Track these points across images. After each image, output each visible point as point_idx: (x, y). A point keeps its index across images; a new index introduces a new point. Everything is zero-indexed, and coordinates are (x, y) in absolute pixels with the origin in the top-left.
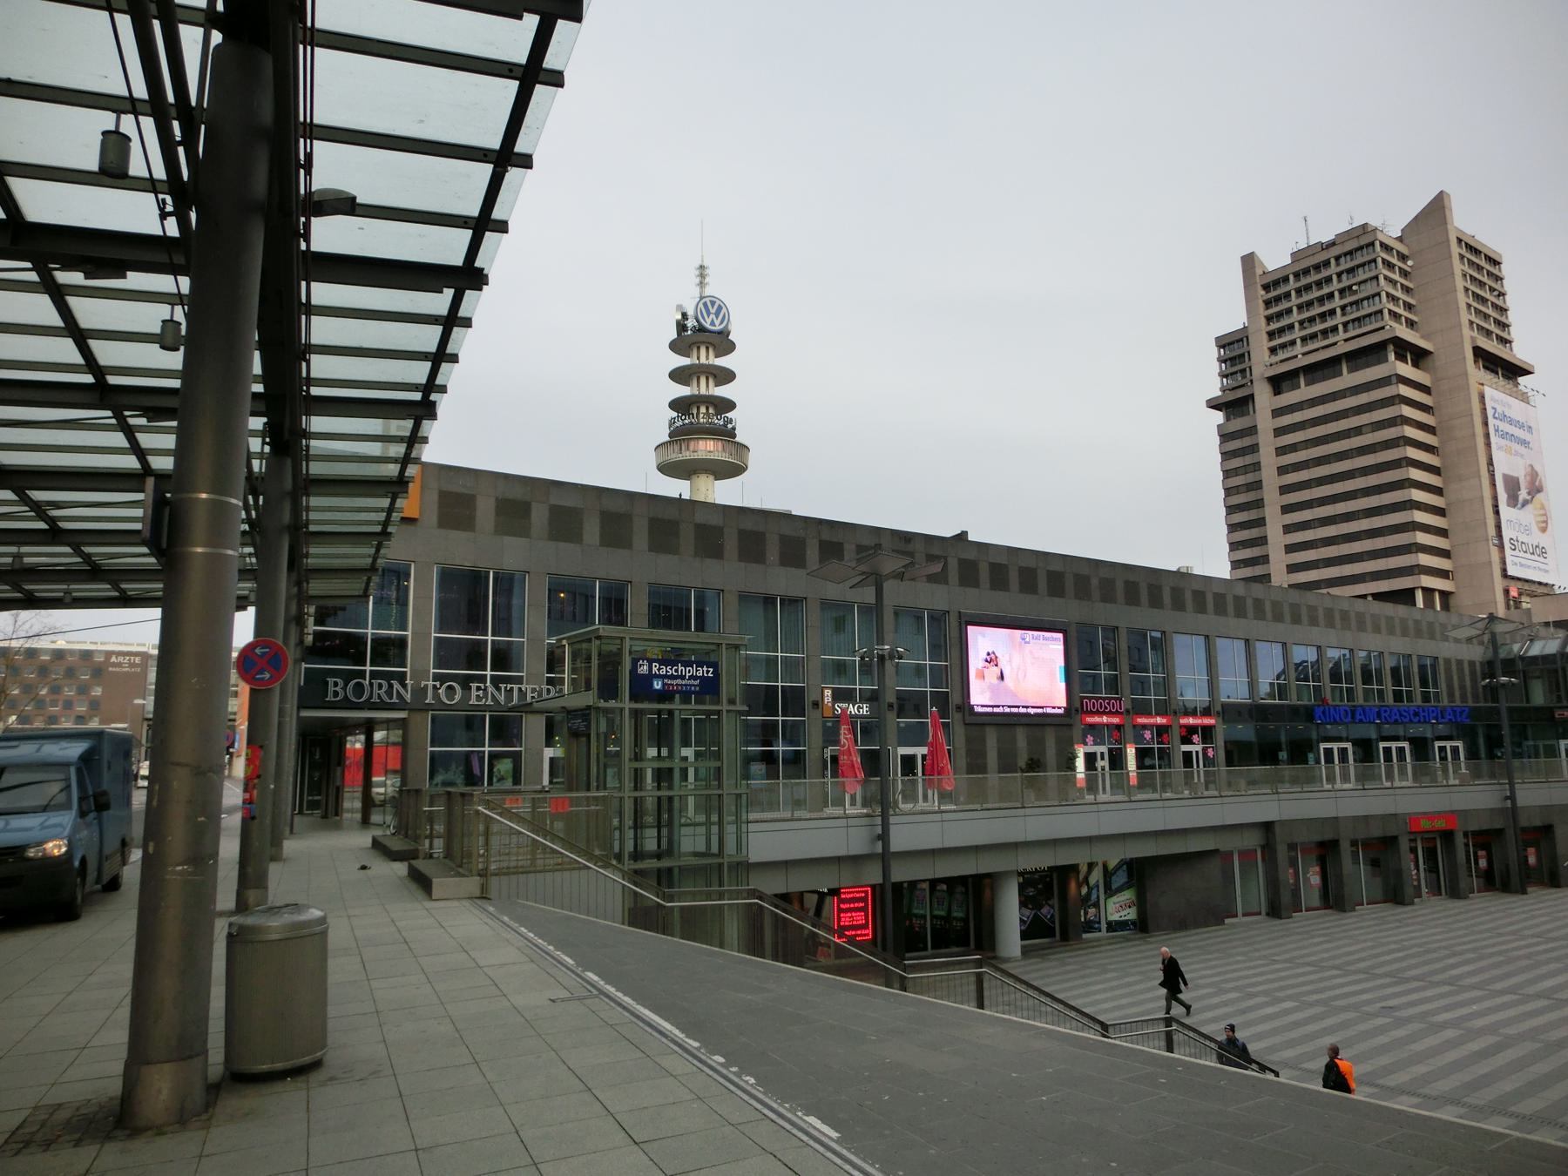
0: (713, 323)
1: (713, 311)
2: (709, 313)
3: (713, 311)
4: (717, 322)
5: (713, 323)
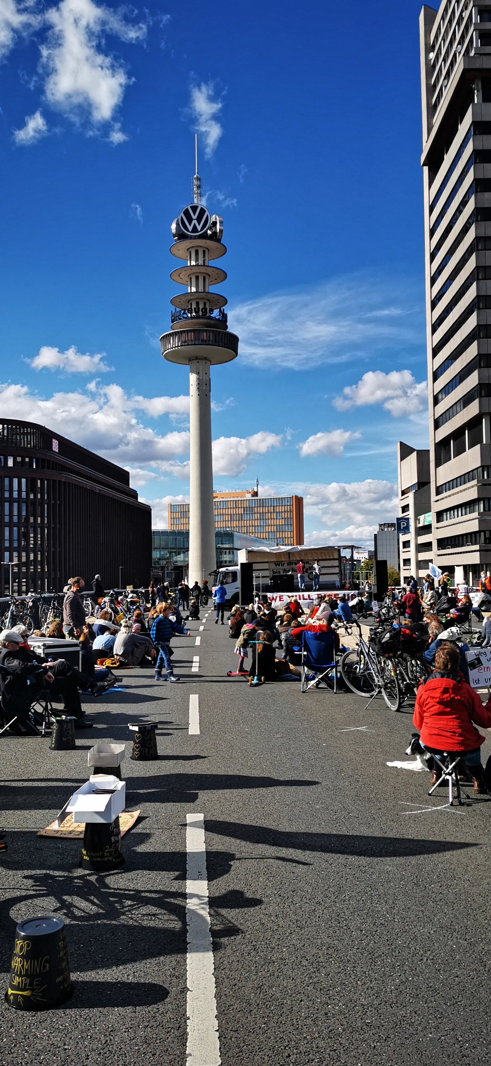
0: (195, 230)
1: (194, 217)
3: (194, 217)
4: (199, 228)
5: (195, 230)
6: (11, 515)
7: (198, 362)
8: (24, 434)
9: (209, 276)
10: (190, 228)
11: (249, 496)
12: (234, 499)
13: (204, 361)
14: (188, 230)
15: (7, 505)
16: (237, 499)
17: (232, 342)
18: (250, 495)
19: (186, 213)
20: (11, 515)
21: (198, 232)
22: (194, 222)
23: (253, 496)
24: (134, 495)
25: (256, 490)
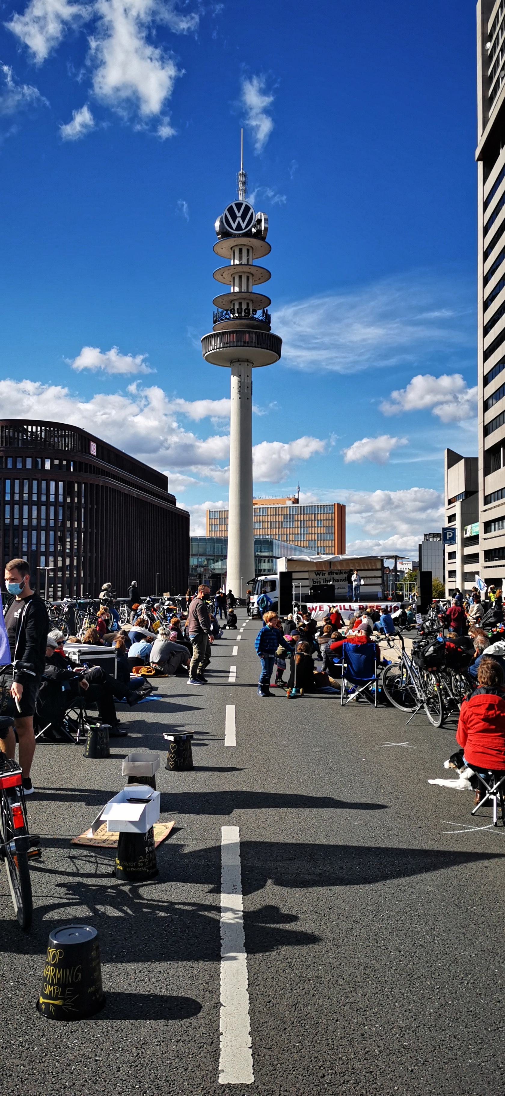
0: (239, 228)
1: (239, 214)
2: (234, 217)
3: (239, 214)
4: (243, 226)
5: (239, 228)
6: (13, 493)
7: (240, 364)
8: (62, 436)
9: (253, 275)
10: (234, 226)
11: (289, 503)
12: (274, 506)
13: (246, 364)
14: (232, 228)
15: (8, 508)
16: (278, 506)
17: (275, 344)
18: (290, 502)
19: (231, 210)
20: (13, 493)
21: (242, 230)
22: (239, 219)
23: (294, 503)
24: (172, 500)
25: (296, 497)
